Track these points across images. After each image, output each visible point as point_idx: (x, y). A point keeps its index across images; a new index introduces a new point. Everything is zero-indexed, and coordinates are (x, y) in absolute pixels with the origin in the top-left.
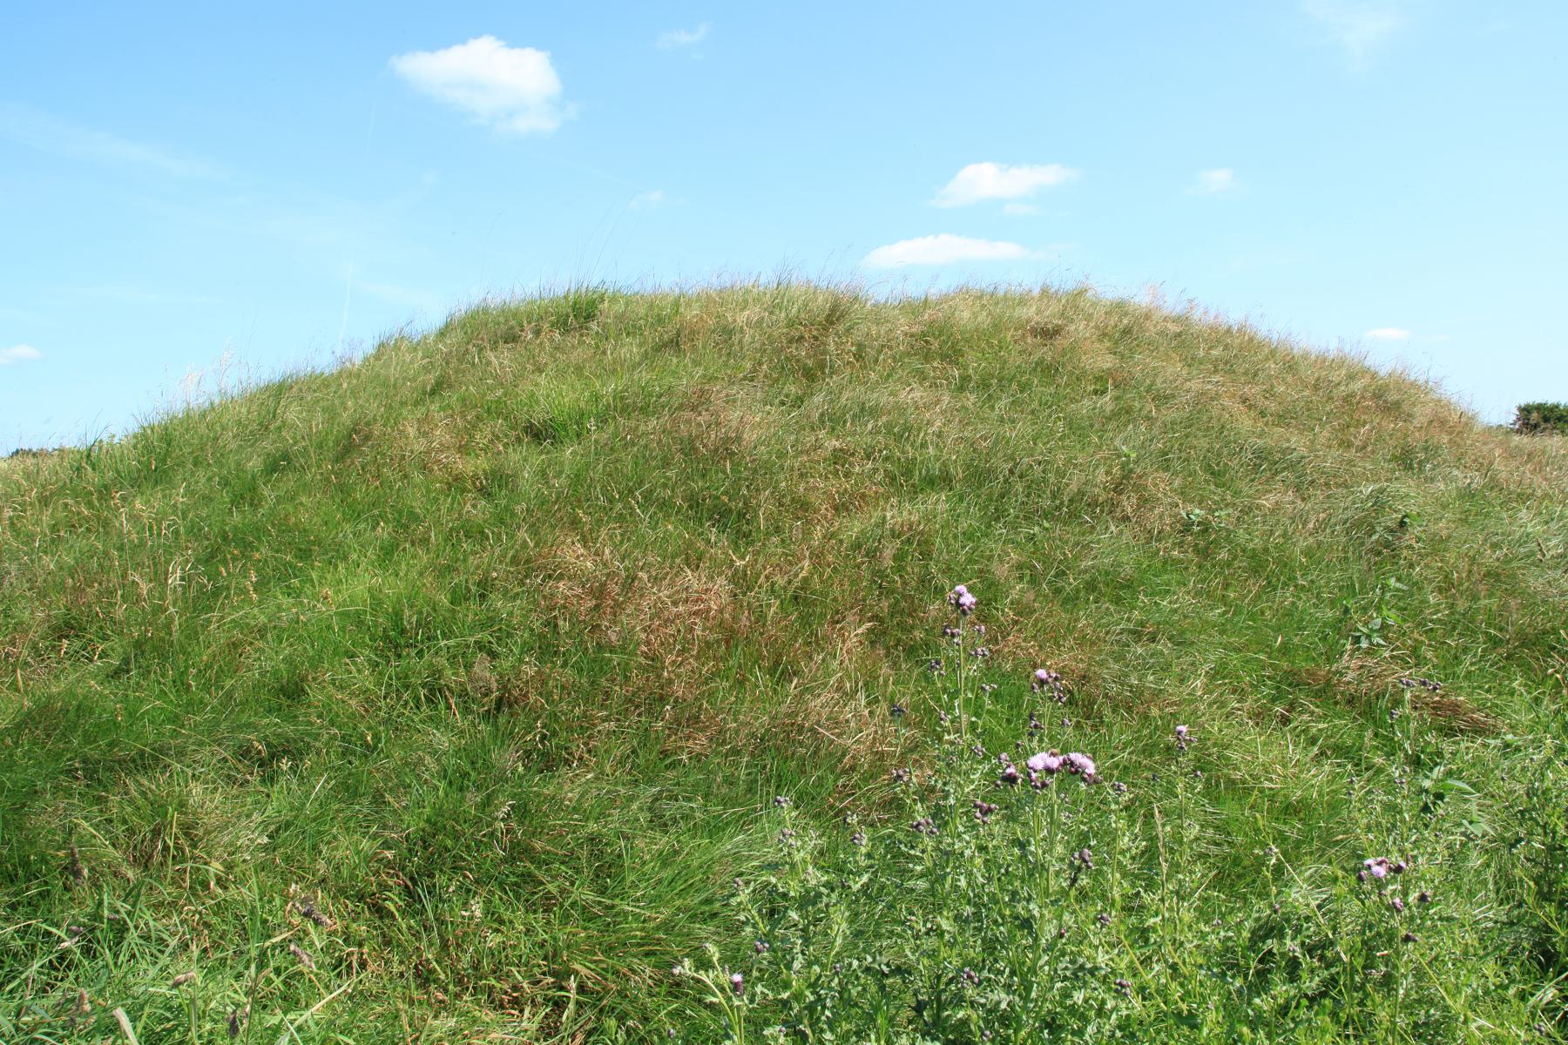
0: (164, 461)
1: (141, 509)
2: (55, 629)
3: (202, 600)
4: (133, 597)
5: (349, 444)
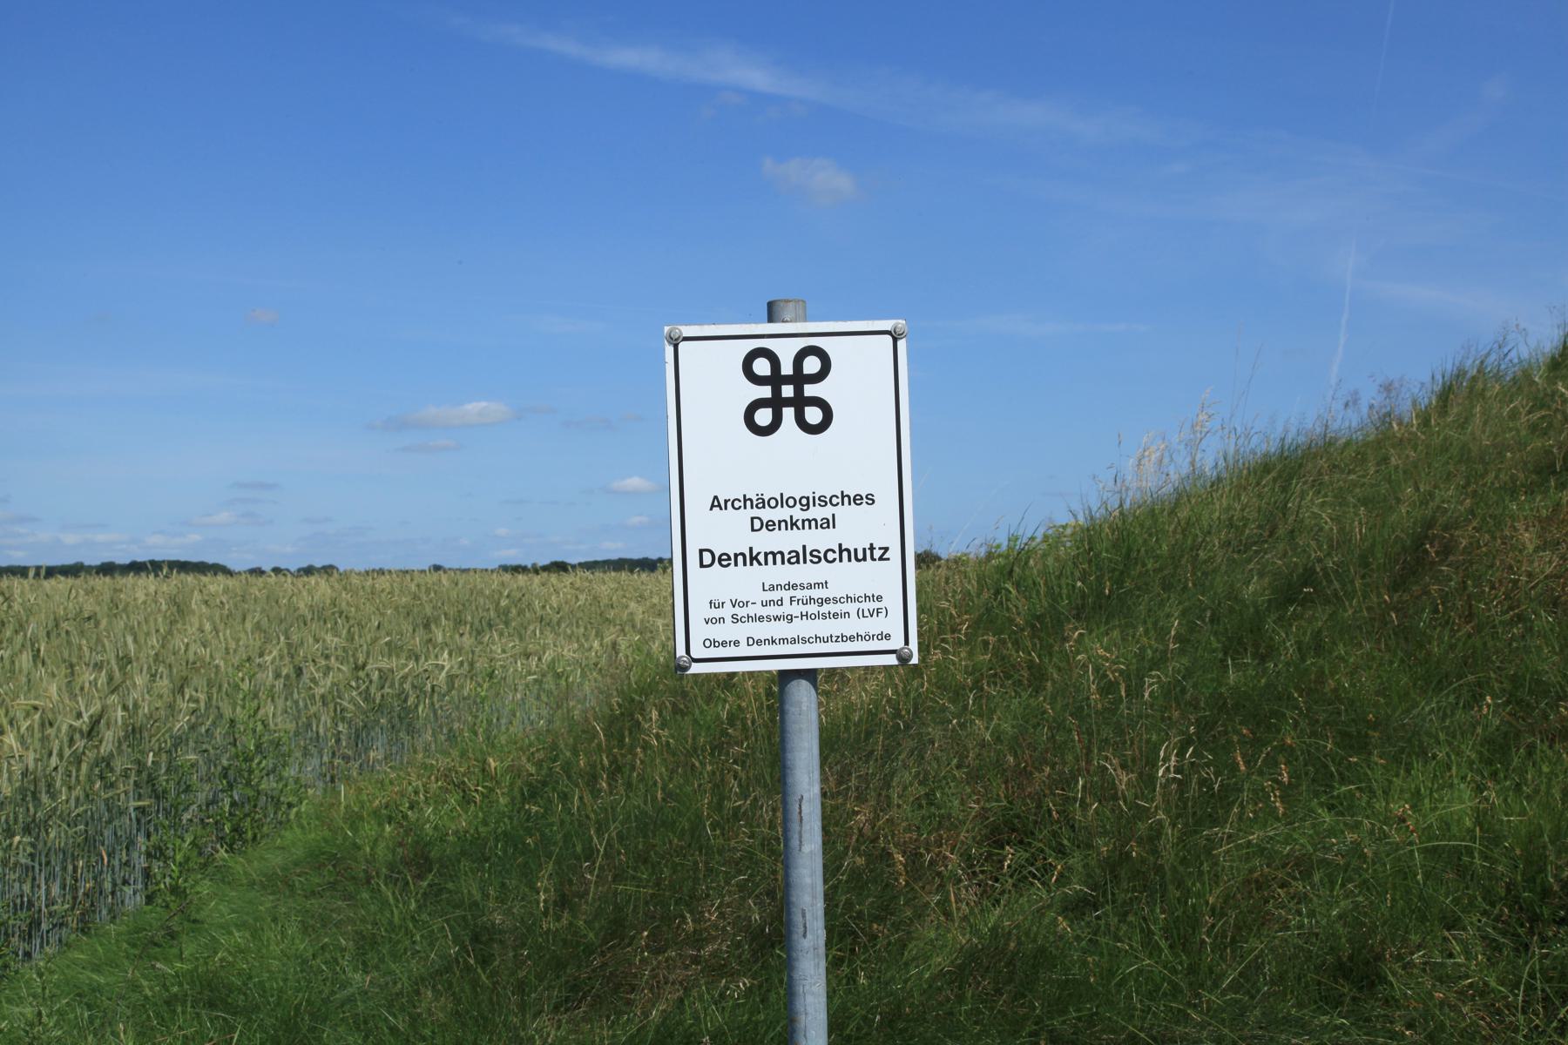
0: (1119, 582)
1: (1096, 651)
2: (995, 830)
3: (1205, 807)
4: (1105, 791)
5: (1415, 559)
